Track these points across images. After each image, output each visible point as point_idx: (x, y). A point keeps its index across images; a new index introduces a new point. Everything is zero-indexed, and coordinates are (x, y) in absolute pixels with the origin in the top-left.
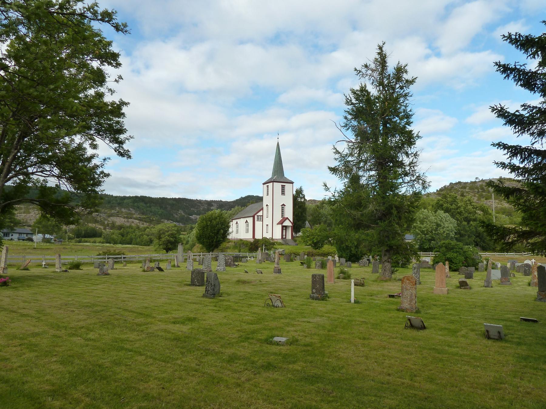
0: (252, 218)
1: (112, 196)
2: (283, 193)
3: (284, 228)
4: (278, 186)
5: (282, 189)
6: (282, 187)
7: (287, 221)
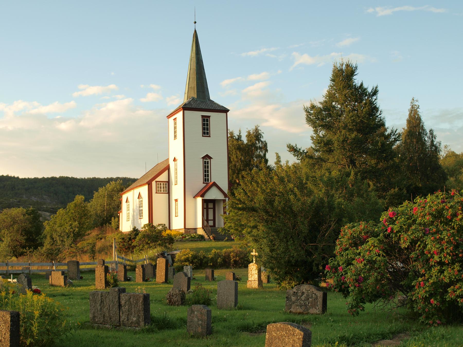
0: (146, 187)
1: (18, 178)
2: (206, 131)
3: (211, 205)
4: (196, 117)
5: (204, 125)
6: (204, 120)
7: (214, 189)
